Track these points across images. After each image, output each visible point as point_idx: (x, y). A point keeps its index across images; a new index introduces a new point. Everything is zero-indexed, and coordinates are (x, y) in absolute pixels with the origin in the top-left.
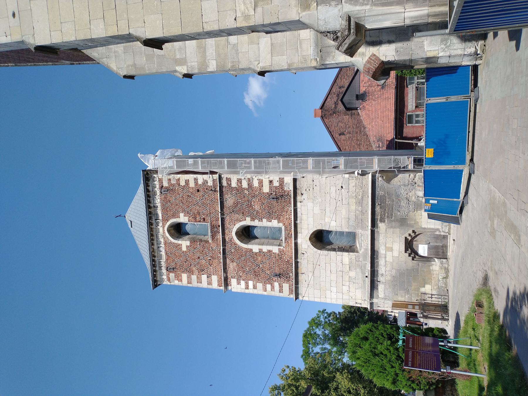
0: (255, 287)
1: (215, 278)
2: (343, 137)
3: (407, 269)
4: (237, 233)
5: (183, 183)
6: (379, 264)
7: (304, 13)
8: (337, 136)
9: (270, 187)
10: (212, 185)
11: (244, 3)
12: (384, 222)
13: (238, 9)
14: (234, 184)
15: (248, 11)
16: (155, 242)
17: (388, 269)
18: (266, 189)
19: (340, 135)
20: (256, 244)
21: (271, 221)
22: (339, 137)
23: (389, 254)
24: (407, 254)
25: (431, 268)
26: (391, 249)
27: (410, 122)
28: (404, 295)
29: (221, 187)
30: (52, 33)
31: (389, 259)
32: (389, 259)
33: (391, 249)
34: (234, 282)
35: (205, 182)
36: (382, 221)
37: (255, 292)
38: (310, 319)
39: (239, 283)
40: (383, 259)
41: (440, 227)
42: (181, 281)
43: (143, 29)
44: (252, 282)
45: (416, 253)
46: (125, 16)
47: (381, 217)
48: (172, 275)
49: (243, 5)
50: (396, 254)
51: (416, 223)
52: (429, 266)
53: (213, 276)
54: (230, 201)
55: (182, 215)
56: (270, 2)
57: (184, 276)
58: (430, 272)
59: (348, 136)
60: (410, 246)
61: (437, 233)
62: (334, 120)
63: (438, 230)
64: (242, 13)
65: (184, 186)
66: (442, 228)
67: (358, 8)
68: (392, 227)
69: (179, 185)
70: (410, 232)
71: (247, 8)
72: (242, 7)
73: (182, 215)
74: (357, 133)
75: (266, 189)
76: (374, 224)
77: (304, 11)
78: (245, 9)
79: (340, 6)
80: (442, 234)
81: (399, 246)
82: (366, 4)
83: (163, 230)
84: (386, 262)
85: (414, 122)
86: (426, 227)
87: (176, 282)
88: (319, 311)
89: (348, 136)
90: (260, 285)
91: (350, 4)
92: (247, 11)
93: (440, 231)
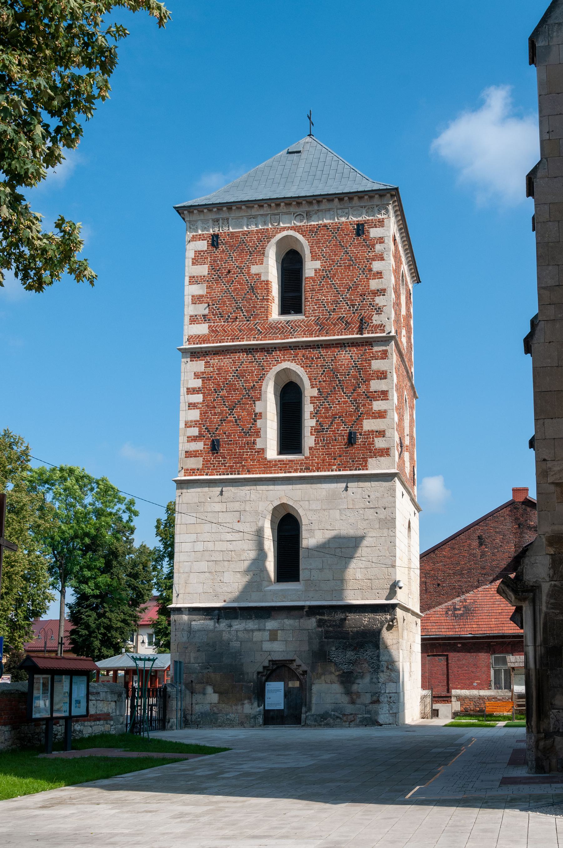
0: (192, 406)
1: (202, 329)
2: (475, 543)
3: (242, 665)
4: (286, 371)
5: (376, 266)
6: (248, 621)
7: (544, 540)
8: (478, 533)
9: (372, 431)
10: (375, 322)
11: (560, 471)
12: (319, 626)
13: (555, 463)
14: (376, 365)
15: (552, 475)
16: (266, 210)
17: (240, 634)
18: (368, 425)
19: (480, 538)
20: (266, 388)
21: (312, 434)
22: (475, 536)
23: (266, 634)
24: (266, 664)
25: (246, 702)
26: (273, 636)
27: (497, 660)
28: (199, 661)
29: (370, 343)
30: (546, 207)
31: (257, 636)
32: (257, 636)
33: (273, 636)
34: (199, 366)
35: (379, 310)
36: (320, 623)
37: (183, 406)
38: (112, 482)
39: (197, 376)
40: (256, 627)
41: (313, 711)
42: (193, 264)
43: (542, 341)
44: (201, 400)
45: (269, 678)
46: (559, 316)
47: (326, 621)
48: (203, 245)
49: (559, 469)
50: (267, 646)
51: (319, 676)
52: (249, 698)
53: (206, 326)
54: (345, 357)
55: (318, 264)
56: (559, 501)
57: (203, 270)
58: (240, 701)
59: (478, 552)
60: (278, 669)
61: (304, 709)
62: (508, 525)
63: (310, 709)
64: (550, 468)
65: (370, 270)
66: (313, 715)
67: (544, 598)
68: (310, 638)
69: (373, 260)
70: (304, 667)
71: (555, 474)
72: (556, 469)
73: (318, 264)
74: (483, 568)
75: (368, 425)
76: (313, 611)
77: (546, 540)
78: (554, 471)
79: (548, 579)
80: (303, 716)
81: (278, 649)
82: (547, 607)
83: (288, 228)
84: (253, 631)
85: (498, 667)
86: (313, 691)
87: (190, 254)
88: (132, 503)
89: (478, 552)
90: (195, 415)
91: (549, 589)
92: (552, 473)
93: (306, 712)
